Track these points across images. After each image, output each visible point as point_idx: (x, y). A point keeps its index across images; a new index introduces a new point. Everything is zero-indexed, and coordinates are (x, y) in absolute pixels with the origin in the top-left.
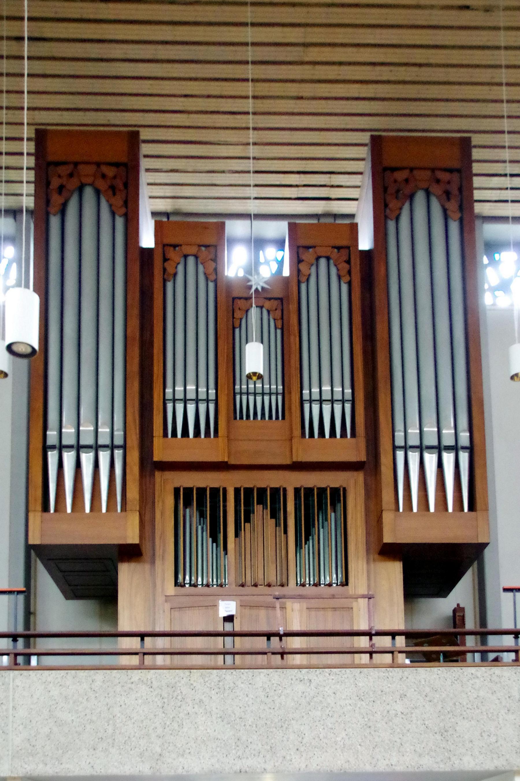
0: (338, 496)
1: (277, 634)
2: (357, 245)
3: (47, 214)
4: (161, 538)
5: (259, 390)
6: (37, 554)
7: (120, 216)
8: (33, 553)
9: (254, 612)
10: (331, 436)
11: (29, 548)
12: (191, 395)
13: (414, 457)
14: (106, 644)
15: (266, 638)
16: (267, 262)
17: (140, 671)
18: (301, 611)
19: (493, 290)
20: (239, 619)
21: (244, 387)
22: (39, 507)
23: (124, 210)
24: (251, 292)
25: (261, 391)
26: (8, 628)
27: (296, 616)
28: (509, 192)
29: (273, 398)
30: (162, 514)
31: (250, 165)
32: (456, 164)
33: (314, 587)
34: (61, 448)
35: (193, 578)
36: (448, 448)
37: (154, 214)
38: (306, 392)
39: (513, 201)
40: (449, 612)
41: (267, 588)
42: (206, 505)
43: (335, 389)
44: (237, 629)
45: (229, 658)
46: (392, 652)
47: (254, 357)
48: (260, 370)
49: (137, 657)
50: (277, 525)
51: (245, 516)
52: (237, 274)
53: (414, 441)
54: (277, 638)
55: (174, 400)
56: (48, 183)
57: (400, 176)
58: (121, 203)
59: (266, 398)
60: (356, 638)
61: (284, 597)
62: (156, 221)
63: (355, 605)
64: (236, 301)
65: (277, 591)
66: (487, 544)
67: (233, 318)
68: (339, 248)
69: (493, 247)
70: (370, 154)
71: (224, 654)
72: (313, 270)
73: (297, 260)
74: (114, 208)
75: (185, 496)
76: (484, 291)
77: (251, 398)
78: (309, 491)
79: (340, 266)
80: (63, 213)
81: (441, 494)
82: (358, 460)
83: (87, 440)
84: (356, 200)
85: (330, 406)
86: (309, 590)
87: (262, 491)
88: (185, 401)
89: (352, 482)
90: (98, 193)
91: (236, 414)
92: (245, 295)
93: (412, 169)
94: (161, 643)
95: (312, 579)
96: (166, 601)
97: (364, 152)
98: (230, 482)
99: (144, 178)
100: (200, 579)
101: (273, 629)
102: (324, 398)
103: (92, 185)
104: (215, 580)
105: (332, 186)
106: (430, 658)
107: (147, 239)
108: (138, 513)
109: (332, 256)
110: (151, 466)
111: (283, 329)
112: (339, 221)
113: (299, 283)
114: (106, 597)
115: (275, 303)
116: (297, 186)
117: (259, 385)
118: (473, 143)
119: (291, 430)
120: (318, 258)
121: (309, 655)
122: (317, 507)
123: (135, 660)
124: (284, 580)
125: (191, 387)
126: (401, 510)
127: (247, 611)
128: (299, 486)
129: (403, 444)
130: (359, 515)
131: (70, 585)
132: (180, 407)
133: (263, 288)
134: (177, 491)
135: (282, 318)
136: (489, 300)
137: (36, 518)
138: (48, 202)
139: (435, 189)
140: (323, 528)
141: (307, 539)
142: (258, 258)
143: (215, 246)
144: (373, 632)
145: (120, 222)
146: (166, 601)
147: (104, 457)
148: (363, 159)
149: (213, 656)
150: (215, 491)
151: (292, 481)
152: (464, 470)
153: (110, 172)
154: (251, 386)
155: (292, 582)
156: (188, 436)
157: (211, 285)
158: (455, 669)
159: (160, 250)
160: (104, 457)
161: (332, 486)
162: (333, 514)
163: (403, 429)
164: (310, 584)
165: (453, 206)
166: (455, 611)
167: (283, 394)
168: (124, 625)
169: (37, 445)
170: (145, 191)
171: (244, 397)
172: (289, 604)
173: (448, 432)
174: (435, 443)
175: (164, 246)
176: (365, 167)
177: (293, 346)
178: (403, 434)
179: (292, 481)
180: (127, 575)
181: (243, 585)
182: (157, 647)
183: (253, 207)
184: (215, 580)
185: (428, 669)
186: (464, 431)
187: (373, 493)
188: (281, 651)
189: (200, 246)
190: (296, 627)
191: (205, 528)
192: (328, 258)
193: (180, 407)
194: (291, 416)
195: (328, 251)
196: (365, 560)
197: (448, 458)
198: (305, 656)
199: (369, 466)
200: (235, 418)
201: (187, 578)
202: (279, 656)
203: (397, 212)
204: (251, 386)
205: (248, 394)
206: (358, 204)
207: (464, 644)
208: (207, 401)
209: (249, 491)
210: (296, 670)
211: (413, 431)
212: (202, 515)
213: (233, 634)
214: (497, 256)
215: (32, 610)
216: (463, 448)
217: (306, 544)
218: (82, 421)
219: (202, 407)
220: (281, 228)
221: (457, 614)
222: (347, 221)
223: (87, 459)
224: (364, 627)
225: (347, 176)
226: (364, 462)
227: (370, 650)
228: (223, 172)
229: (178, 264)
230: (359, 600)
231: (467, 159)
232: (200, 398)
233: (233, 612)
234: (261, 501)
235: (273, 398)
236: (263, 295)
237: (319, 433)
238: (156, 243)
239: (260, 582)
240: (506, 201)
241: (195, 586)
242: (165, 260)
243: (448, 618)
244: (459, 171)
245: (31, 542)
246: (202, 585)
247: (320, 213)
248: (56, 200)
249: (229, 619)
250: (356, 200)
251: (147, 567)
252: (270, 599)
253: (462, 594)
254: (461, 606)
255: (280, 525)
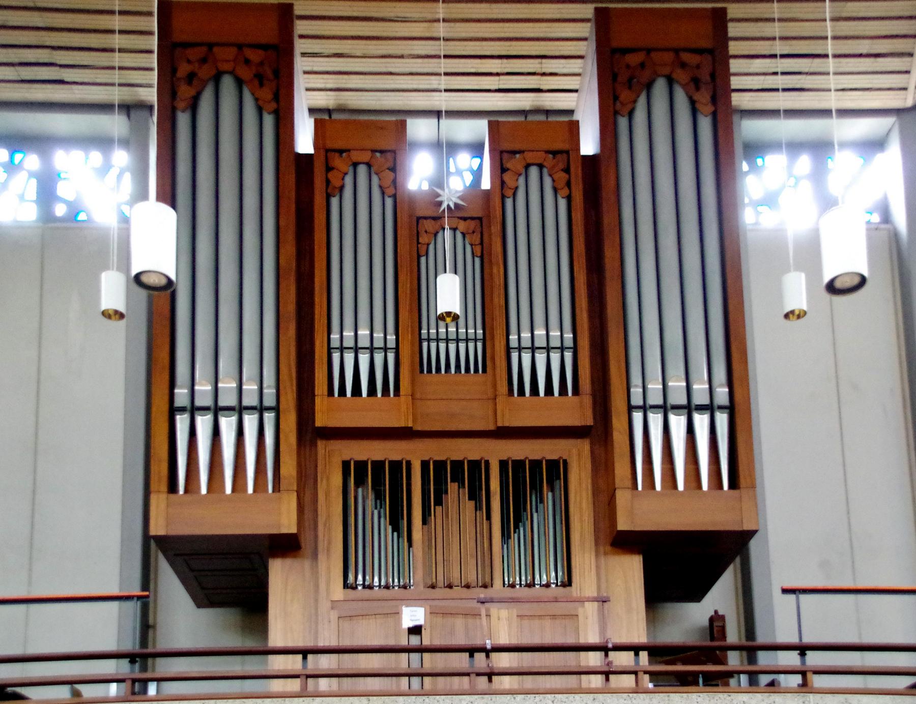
0: (556, 470)
1: (483, 649)
2: (578, 149)
3: (174, 110)
4: (325, 525)
5: (452, 336)
6: (157, 547)
7: (269, 113)
8: (153, 544)
9: (450, 620)
10: (353, 394)
11: (147, 538)
12: (364, 342)
13: (656, 421)
14: (251, 665)
15: (467, 654)
16: (459, 173)
17: (301, 699)
18: (509, 619)
19: (757, 204)
20: (428, 630)
21: (433, 331)
22: (164, 487)
23: (274, 105)
24: (442, 209)
25: (464, 337)
26: (118, 645)
27: (502, 626)
28: (779, 77)
29: (471, 345)
30: (327, 494)
31: (441, 48)
32: (705, 44)
33: (527, 588)
34: (194, 410)
35: (367, 578)
36: (701, 408)
37: (312, 111)
38: (513, 337)
39: (784, 90)
40: (705, 622)
41: (465, 590)
42: (384, 483)
43: (551, 334)
44: (426, 642)
45: (416, 681)
46: (635, 673)
47: (448, 293)
48: (457, 309)
49: (298, 681)
50: (478, 508)
51: (435, 496)
52: (420, 186)
53: (655, 398)
54: (483, 655)
55: (342, 349)
56: (174, 71)
57: (634, 59)
58: (270, 96)
59: (462, 346)
60: (583, 654)
61: (492, 601)
62: (316, 121)
63: (580, 611)
64: (421, 221)
65: (482, 594)
66: (755, 532)
67: (418, 243)
68: (555, 153)
69: (755, 149)
70: (594, 33)
71: (409, 675)
72: (522, 180)
73: (500, 169)
74: (260, 103)
75: (356, 472)
76: (744, 205)
77: (442, 346)
78: (519, 465)
79: (556, 176)
80: (193, 108)
81: (692, 467)
82: (583, 424)
83: (228, 399)
84: (576, 91)
85: (545, 355)
86: (520, 592)
87: (457, 465)
88: (356, 350)
89: (574, 451)
90: (240, 83)
91: (422, 366)
92: (435, 215)
93: (649, 51)
94: (325, 662)
95: (523, 578)
96: (332, 608)
97: (586, 30)
98: (414, 453)
99: (300, 64)
100: (376, 579)
101: (478, 642)
102: (537, 344)
103: (231, 73)
104: (396, 580)
105: (544, 74)
106: (685, 681)
107: (304, 143)
108: (295, 494)
109: (545, 164)
110: (310, 434)
111: (483, 256)
112: (552, 119)
113: (503, 197)
114: (252, 604)
115: (472, 224)
116: (498, 74)
117: (452, 329)
118: (730, 16)
119: (495, 386)
120: (527, 166)
121: (521, 677)
122: (528, 486)
123: (294, 685)
124: (488, 579)
125: (364, 332)
126: (640, 488)
127: (439, 620)
128: (427, 458)
129: (641, 403)
130: (584, 494)
131: (203, 588)
132: (349, 358)
133: (456, 205)
134: (346, 465)
135: (482, 243)
136: (753, 218)
137: (159, 501)
138: (174, 95)
139: (680, 75)
140: (537, 511)
141: (516, 527)
142: (444, 167)
143: (394, 152)
144: (610, 645)
145: (269, 121)
146: (332, 608)
147: (250, 422)
148: (585, 39)
149: (394, 678)
150: (396, 466)
151: (496, 452)
152: (723, 435)
153: (254, 56)
154: (442, 330)
155: (498, 582)
156: (361, 395)
157: (389, 202)
158: (721, 695)
159: (322, 158)
160: (250, 422)
161: (437, 458)
162: (550, 494)
163: (640, 384)
164: (521, 585)
165: (703, 97)
166: (712, 620)
167: (484, 340)
168: (276, 639)
169: (160, 405)
170: (300, 82)
171: (433, 345)
172: (494, 609)
173: (700, 387)
174: (683, 401)
175: (327, 151)
176: (588, 49)
177: (496, 280)
178: (641, 390)
179: (496, 452)
180: (281, 576)
181: (433, 587)
182: (320, 667)
183: (442, 101)
184: (396, 580)
185: (685, 695)
186: (721, 386)
187: (602, 467)
188: (488, 671)
189: (374, 151)
190: (504, 639)
191: (382, 514)
192: (541, 166)
193: (349, 358)
194: (494, 368)
195: (539, 157)
196: (593, 554)
197: (701, 421)
198: (516, 677)
199: (599, 432)
200: (422, 371)
201: (360, 577)
202: (485, 678)
203: (629, 107)
204: (442, 330)
205: (438, 340)
206: (578, 97)
207: (723, 661)
208: (562, 349)
209: (440, 465)
210: (509, 697)
211: (655, 386)
212: (379, 496)
213: (421, 650)
214: (759, 161)
215: (151, 622)
216: (721, 408)
217: (515, 532)
218: (221, 376)
219: (379, 358)
220: (479, 129)
221: (715, 624)
222: (565, 119)
223: (227, 424)
224: (593, 638)
225: (563, 61)
226: (590, 427)
227: (606, 669)
228: (402, 57)
229: (346, 174)
230: (586, 604)
231: (722, 38)
232: (360, 345)
233: (421, 622)
234: (457, 477)
235: (471, 345)
236: (456, 211)
237: (531, 390)
238: (316, 146)
239: (456, 581)
240: (777, 90)
241: (371, 587)
242: (329, 169)
243: (702, 629)
244: (710, 51)
245: (153, 531)
246: (380, 586)
247: (528, 108)
248: (185, 91)
249: (416, 630)
250: (576, 91)
251: (307, 563)
252: (474, 604)
253: (720, 597)
254: (720, 613)
255: (481, 509)
